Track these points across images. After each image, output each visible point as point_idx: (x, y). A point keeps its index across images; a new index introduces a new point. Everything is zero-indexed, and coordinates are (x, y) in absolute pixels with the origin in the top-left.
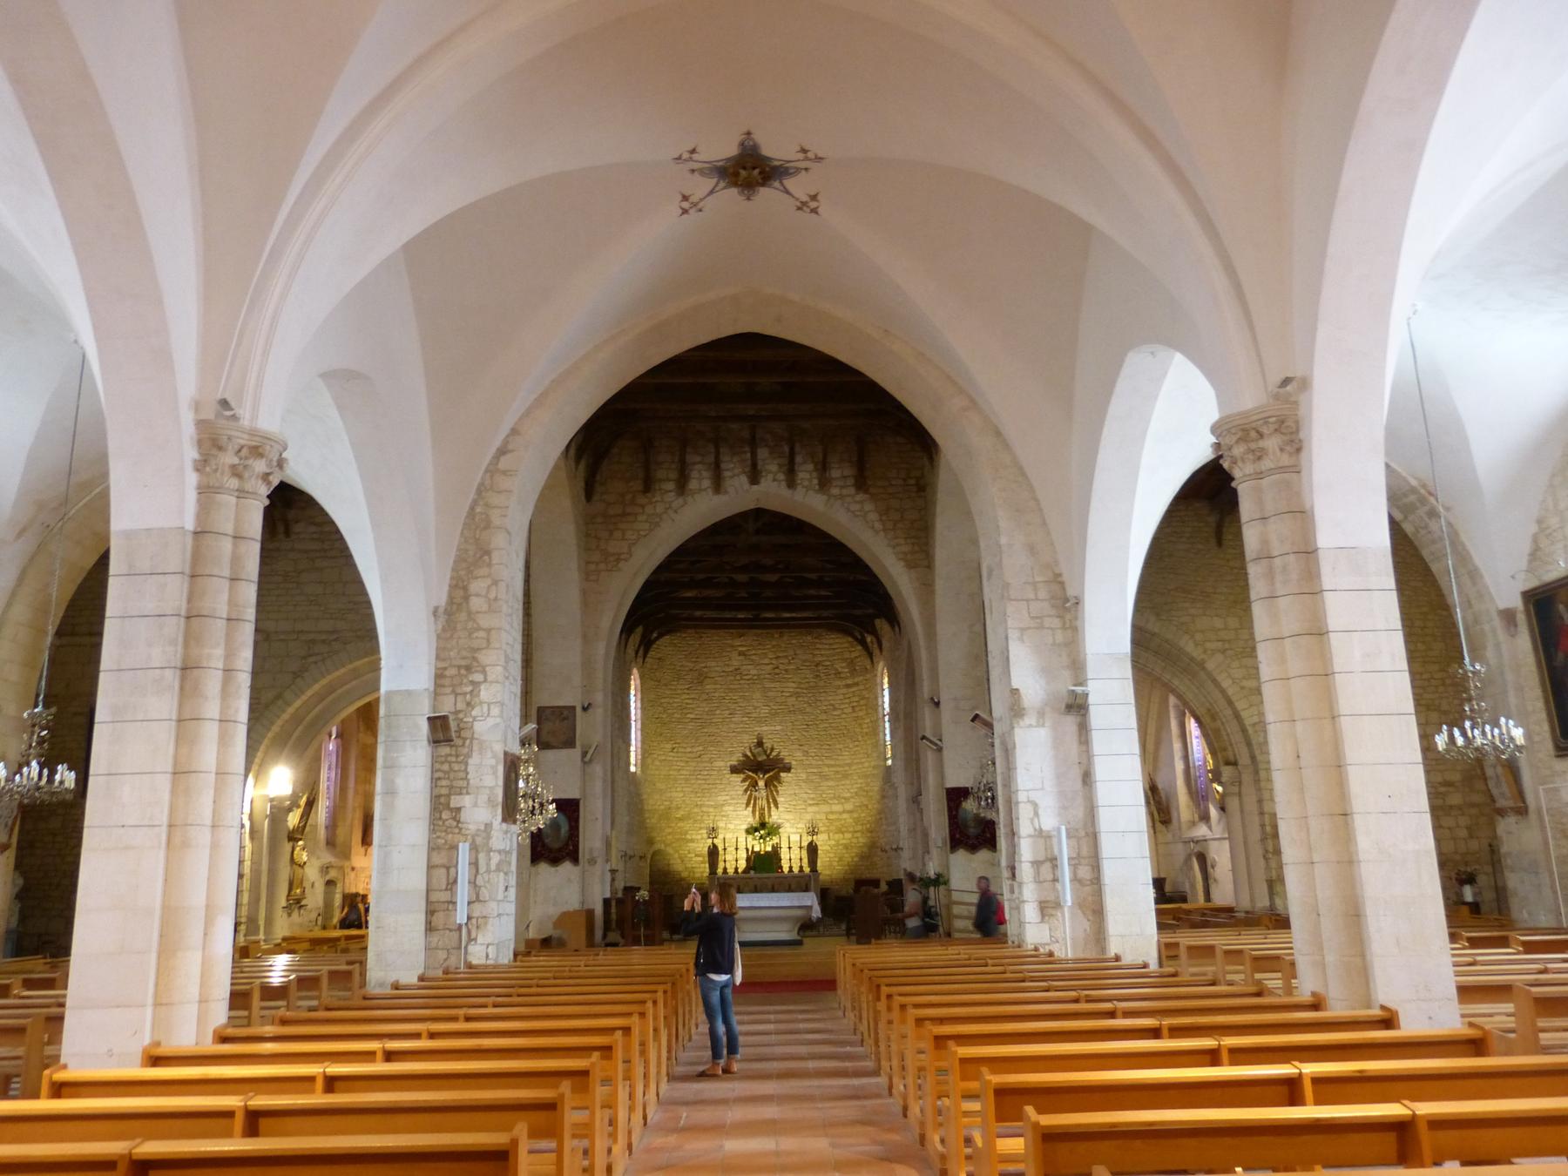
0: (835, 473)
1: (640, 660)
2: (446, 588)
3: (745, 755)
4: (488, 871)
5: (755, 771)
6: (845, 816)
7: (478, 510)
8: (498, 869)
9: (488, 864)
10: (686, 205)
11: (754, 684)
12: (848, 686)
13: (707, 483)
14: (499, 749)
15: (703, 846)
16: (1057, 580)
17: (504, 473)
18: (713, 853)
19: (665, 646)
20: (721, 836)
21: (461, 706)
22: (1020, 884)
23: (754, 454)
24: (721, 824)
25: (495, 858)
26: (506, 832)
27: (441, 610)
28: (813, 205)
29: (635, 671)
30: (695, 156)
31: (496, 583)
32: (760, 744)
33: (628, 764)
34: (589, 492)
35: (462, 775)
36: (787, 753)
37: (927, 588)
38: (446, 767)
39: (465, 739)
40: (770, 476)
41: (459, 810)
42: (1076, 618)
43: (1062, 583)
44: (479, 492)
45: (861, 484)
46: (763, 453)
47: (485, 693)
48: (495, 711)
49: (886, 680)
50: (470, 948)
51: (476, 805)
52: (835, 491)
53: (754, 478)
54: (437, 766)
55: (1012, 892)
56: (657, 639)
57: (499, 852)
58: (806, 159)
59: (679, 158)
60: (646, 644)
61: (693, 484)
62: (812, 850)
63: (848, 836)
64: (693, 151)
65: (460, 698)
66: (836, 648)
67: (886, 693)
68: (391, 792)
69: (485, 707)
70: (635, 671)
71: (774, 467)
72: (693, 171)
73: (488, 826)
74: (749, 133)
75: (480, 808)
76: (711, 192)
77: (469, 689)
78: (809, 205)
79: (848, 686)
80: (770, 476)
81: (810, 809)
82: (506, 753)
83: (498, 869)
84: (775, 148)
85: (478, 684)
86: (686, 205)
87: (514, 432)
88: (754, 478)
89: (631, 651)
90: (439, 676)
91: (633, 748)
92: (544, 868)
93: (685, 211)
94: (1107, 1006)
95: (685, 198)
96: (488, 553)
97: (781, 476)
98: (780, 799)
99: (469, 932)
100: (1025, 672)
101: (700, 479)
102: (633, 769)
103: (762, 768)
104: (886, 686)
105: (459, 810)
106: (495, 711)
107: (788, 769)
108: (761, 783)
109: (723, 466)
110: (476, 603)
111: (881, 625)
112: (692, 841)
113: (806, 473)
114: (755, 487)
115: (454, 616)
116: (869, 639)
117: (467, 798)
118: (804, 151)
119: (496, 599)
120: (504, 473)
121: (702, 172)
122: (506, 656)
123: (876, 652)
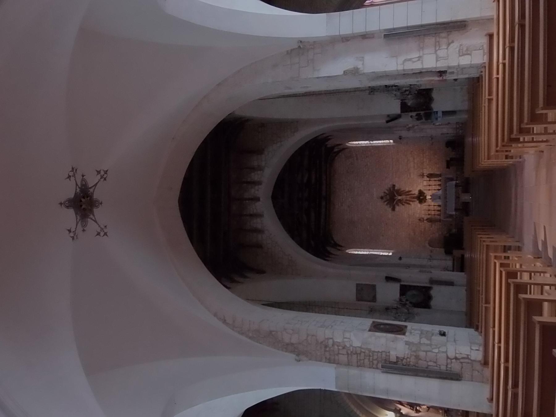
0: (255, 164)
1: (343, 249)
2: (287, 354)
3: (387, 204)
4: (431, 345)
5: (394, 200)
6: (416, 161)
7: (251, 335)
8: (430, 340)
9: (427, 345)
10: (102, 234)
11: (354, 199)
12: (357, 159)
13: (259, 220)
14: (367, 334)
15: (428, 224)
16: (290, 53)
17: (234, 321)
18: (430, 220)
19: (337, 238)
20: (423, 216)
21: (344, 352)
22: (449, 67)
23: (246, 199)
24: (418, 216)
25: (424, 341)
26: (411, 333)
27: (297, 358)
28: (102, 173)
29: (347, 251)
30: (73, 230)
31: (285, 329)
32: (382, 198)
33: (388, 256)
34: (261, 272)
35: (379, 354)
36: (387, 184)
37: (307, 122)
38: (375, 362)
39: (361, 352)
40: (256, 192)
41: (397, 357)
42: (308, 42)
43: (292, 50)
44: (242, 334)
45: (259, 151)
46: (246, 195)
47: (338, 339)
48: (347, 335)
49: (354, 142)
50: (472, 358)
51: (396, 349)
52: (263, 164)
53: (257, 199)
54: (374, 366)
55: (453, 73)
56: (334, 241)
57: (421, 338)
58: (74, 176)
59: (73, 238)
60: (336, 245)
61: (259, 226)
62: (430, 176)
63: (425, 160)
64: (70, 231)
65: (341, 352)
66: (341, 165)
67: (360, 142)
68: (387, 392)
69: (345, 340)
70: (347, 251)
71: (253, 191)
72: (84, 230)
73: (407, 343)
74: (61, 204)
75: (397, 346)
76: (95, 221)
77: (336, 347)
78: (103, 175)
79: (357, 159)
80: (256, 192)
81: (412, 176)
82: (370, 331)
83: (430, 340)
84: (70, 191)
85: (333, 341)
86: (102, 234)
87: (215, 315)
88: (257, 199)
89: (338, 253)
90: (330, 361)
91: (381, 254)
92: (433, 303)
93: (105, 234)
94: (501, 66)
95: (98, 234)
96: (271, 332)
97: (257, 187)
98: (407, 190)
99: (463, 358)
100: (334, 69)
101: (257, 223)
102: (391, 254)
103: (393, 197)
104: (357, 142)
105: (397, 357)
106: (347, 335)
107: (394, 186)
108: (400, 198)
109: (252, 213)
110: (294, 340)
111: (330, 144)
112: (425, 229)
113: (255, 176)
114: (261, 199)
115: (300, 351)
116: (336, 150)
117: (392, 353)
118: (69, 177)
119: (293, 330)
120: (234, 321)
121: (84, 226)
122: (321, 327)
123: (341, 147)
